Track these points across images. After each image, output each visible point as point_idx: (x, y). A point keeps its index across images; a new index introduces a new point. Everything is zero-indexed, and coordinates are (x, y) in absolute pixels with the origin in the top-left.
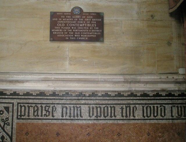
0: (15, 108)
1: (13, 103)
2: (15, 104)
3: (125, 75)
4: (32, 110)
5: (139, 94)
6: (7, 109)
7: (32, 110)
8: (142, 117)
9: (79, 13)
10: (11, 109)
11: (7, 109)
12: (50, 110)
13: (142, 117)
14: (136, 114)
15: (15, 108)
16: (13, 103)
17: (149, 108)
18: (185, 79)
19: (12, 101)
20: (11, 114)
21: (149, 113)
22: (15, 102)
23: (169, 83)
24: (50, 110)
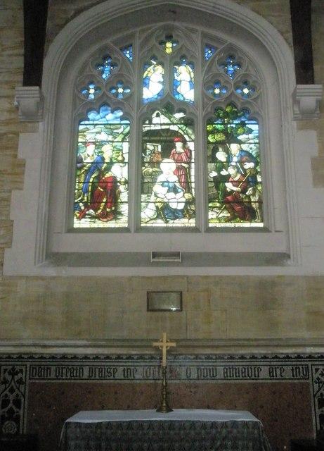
0: (28, 369)
1: (26, 365)
2: (28, 366)
4: (97, 370)
5: (248, 357)
6: (21, 371)
7: (97, 370)
8: (84, 368)
9: (155, 216)
10: (24, 370)
11: (21, 371)
12: (112, 371)
13: (84, 368)
14: (116, 375)
15: (28, 369)
16: (308, 378)
19: (26, 363)
20: (24, 375)
21: (34, 374)
22: (28, 364)
24: (112, 371)
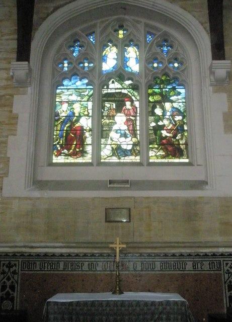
0: (20, 263)
1: (19, 261)
2: (20, 261)
3: (38, 108)
4: (70, 264)
6: (15, 265)
7: (70, 264)
9: (111, 154)
10: (17, 264)
11: (15, 265)
12: (80, 265)
14: (83, 268)
15: (20, 263)
16: (221, 270)
17: (179, 268)
18: (48, 319)
19: (19, 259)
20: (17, 267)
22: (20, 260)
23: (161, 182)
24: (80, 265)
